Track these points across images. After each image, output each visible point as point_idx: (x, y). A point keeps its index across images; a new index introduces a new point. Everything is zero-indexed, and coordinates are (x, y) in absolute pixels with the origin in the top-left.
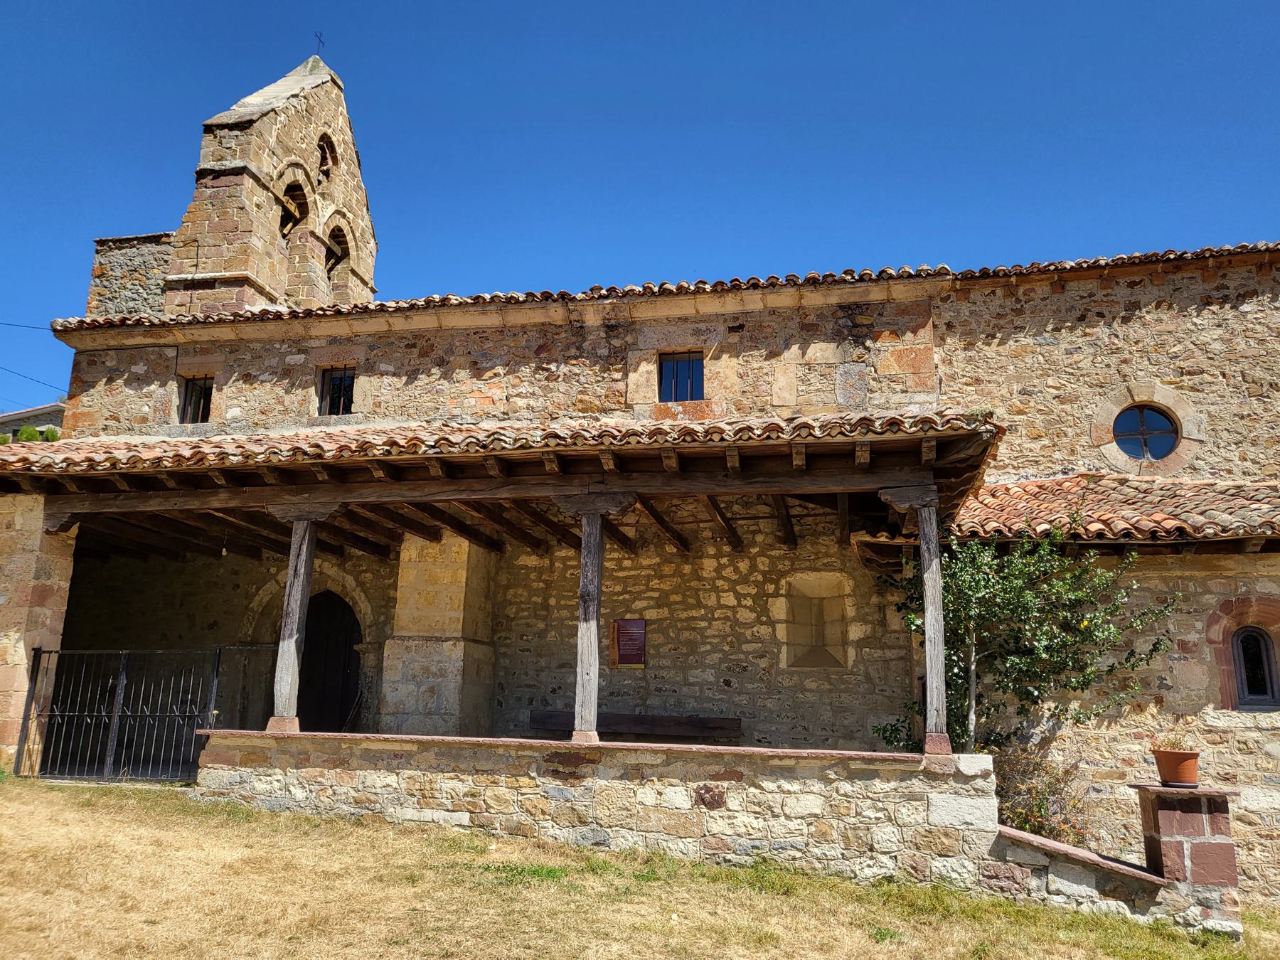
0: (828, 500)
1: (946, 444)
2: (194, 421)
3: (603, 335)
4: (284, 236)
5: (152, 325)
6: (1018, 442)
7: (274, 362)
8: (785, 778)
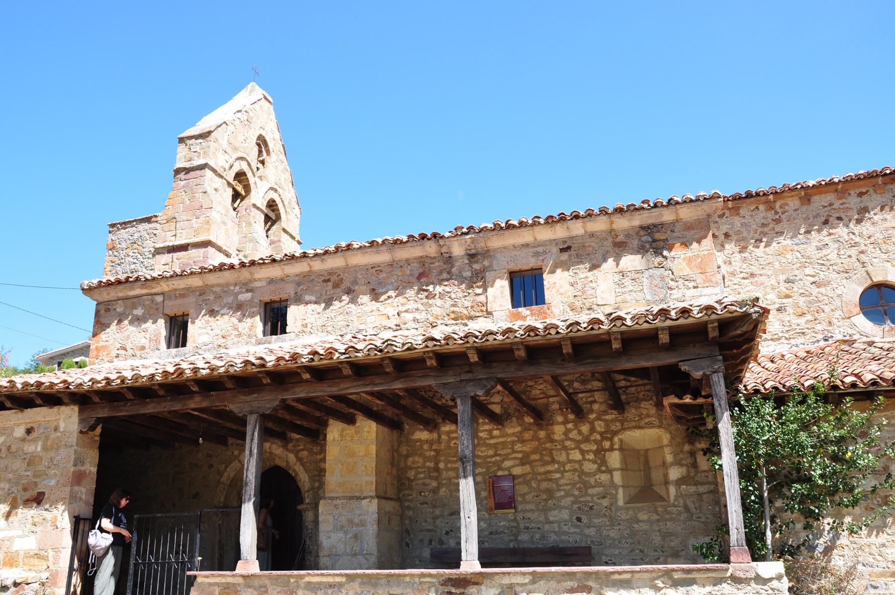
0: (643, 373)
1: (725, 324)
2: (177, 346)
3: (467, 261)
4: (235, 209)
5: (147, 280)
6: (788, 319)
7: (230, 299)
8: (624, 588)
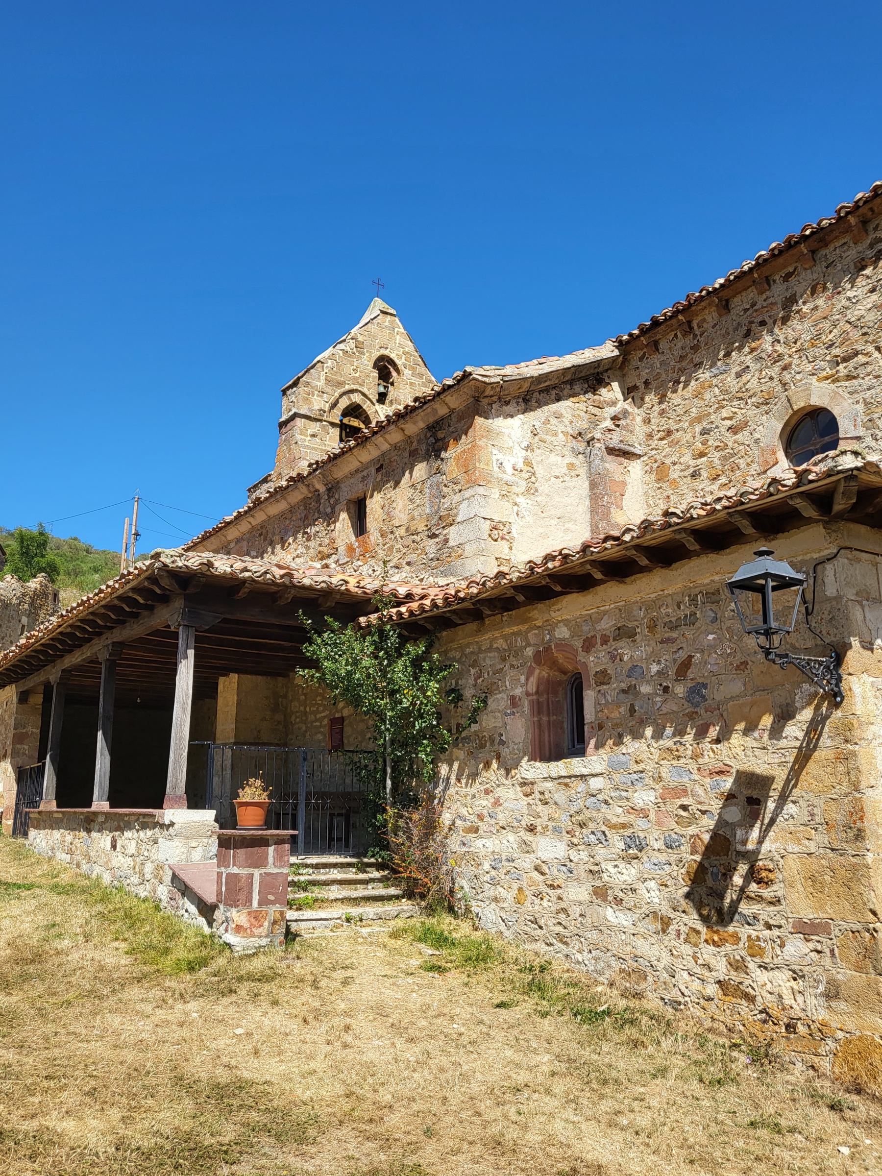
6: (701, 487)
